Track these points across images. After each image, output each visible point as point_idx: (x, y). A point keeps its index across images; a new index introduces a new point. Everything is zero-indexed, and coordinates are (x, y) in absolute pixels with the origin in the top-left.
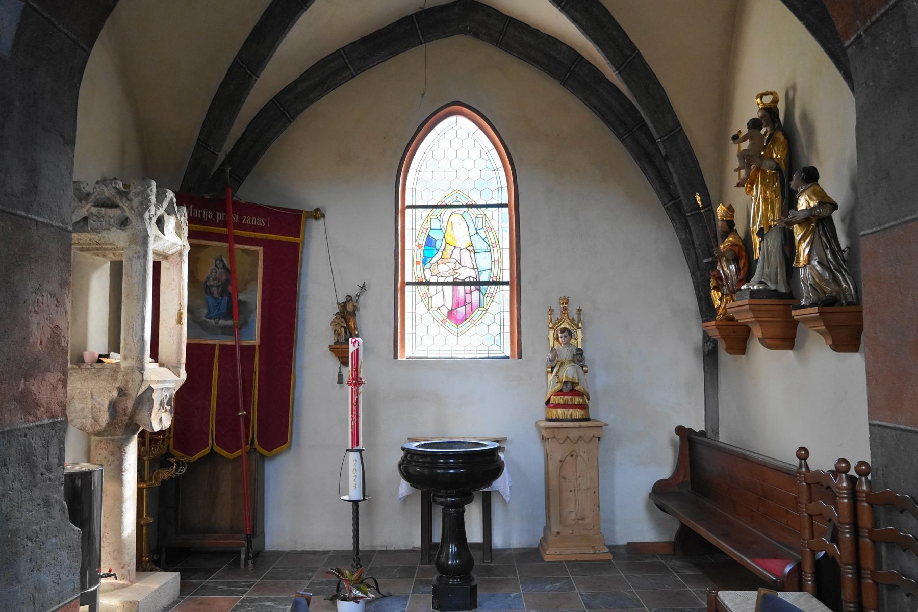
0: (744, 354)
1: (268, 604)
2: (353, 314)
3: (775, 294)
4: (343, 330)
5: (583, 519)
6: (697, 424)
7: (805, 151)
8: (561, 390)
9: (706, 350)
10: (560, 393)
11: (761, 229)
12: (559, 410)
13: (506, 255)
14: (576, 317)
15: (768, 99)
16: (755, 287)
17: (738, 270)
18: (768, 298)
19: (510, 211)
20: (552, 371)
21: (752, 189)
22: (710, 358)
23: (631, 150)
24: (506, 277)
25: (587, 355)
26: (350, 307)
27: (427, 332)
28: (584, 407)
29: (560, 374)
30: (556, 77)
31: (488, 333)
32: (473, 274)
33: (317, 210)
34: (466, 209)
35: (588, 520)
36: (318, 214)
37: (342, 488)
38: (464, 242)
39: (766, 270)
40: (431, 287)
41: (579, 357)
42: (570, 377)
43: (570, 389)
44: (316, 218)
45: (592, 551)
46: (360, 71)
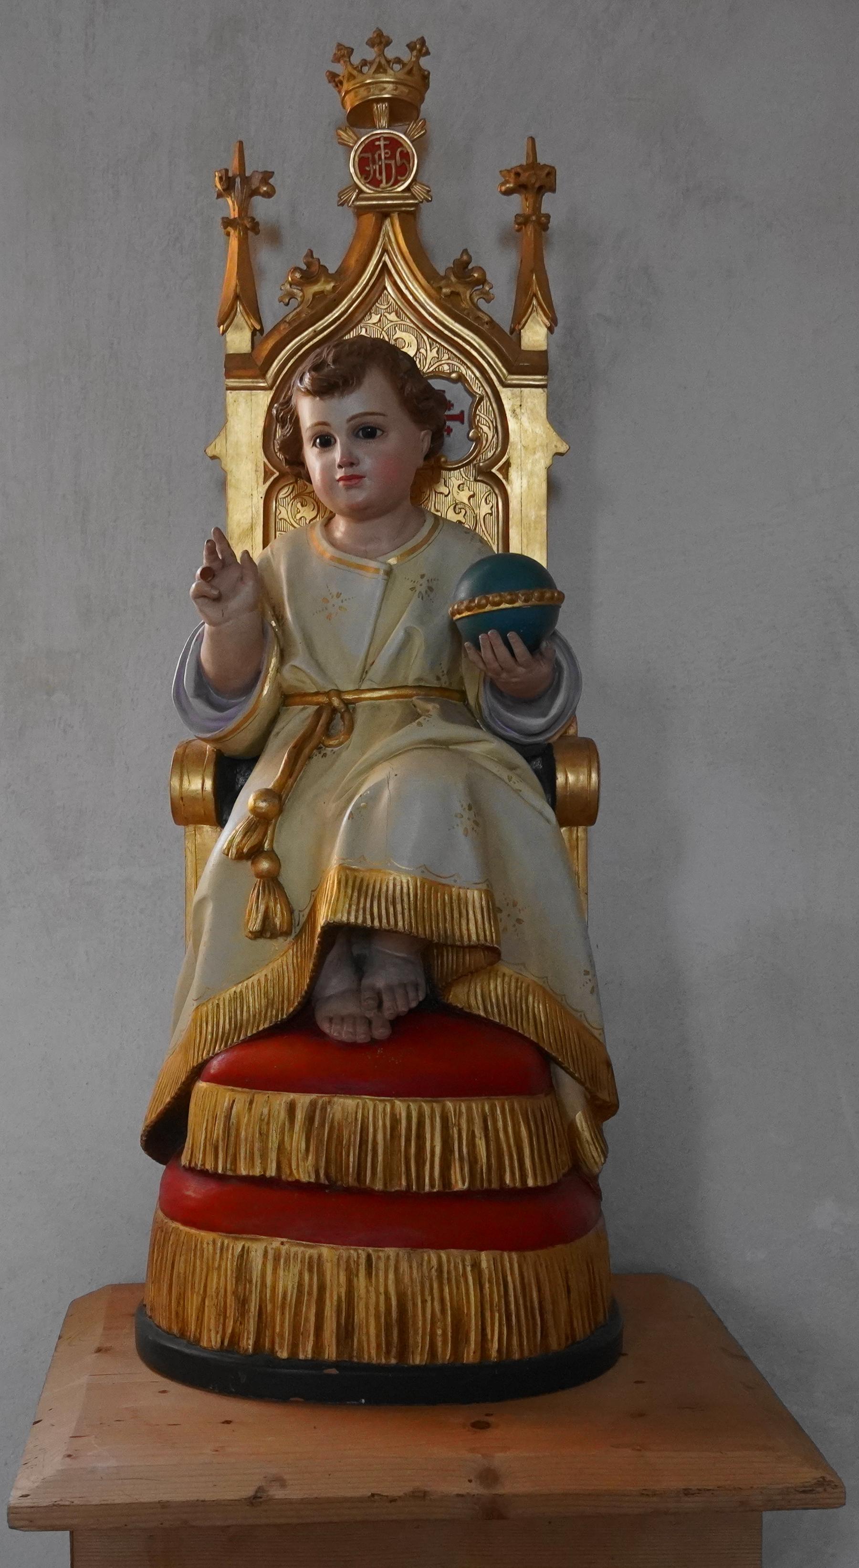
6: (233, 167)
8: (299, 1022)
10: (285, 1048)
14: (500, 268)
25: (600, 634)
28: (546, 1212)
29: (290, 840)
41: (508, 647)
42: (399, 878)
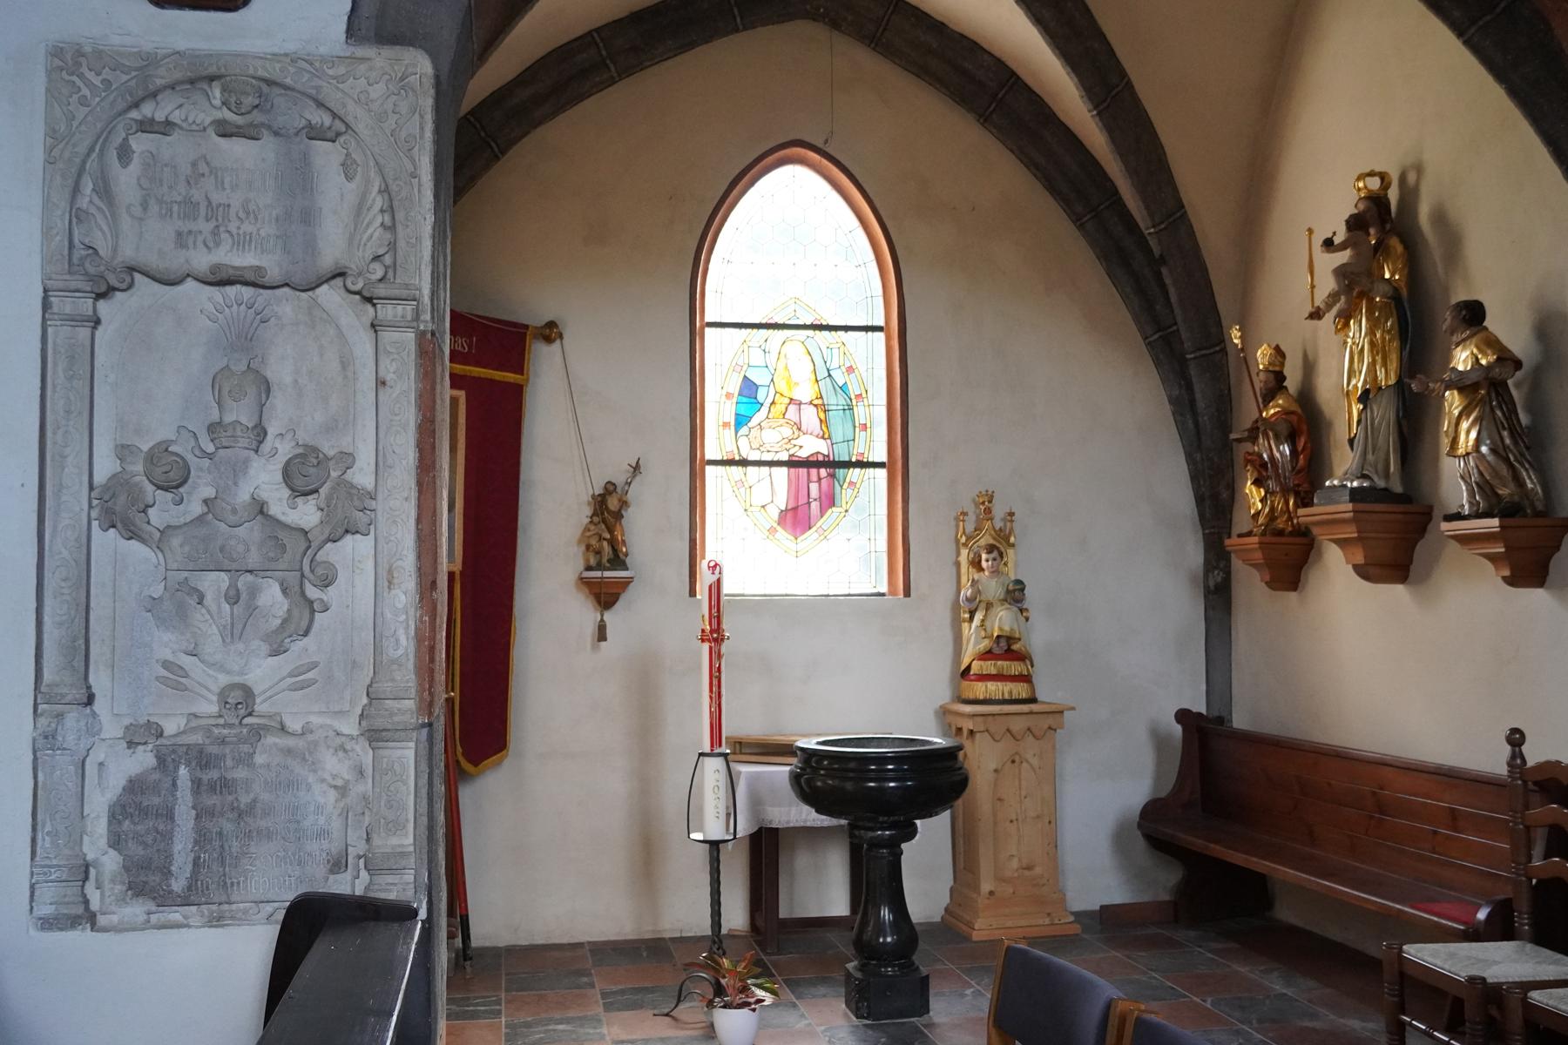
0: (1295, 589)
1: (561, 1027)
2: (618, 516)
3: (1385, 495)
4: (605, 544)
5: (1029, 868)
7: (1440, 270)
8: (989, 652)
9: (1212, 584)
10: (987, 655)
11: (1366, 392)
12: (989, 684)
13: (881, 414)
15: (1374, 184)
16: (1355, 484)
17: (1294, 452)
18: (1377, 501)
19: (888, 339)
20: (971, 619)
21: (1347, 325)
22: (1218, 596)
23: (1093, 244)
24: (880, 454)
26: (613, 503)
27: (748, 545)
28: (1026, 679)
29: (988, 623)
30: (971, 110)
31: (848, 553)
32: (822, 447)
33: (552, 325)
34: (810, 333)
35: (1038, 870)
36: (550, 332)
37: (691, 818)
38: (806, 392)
39: (1370, 457)
40: (750, 469)
41: (1015, 595)
42: (1007, 628)
43: (1007, 649)
44: (549, 340)
45: (1047, 921)
46: (626, 72)
